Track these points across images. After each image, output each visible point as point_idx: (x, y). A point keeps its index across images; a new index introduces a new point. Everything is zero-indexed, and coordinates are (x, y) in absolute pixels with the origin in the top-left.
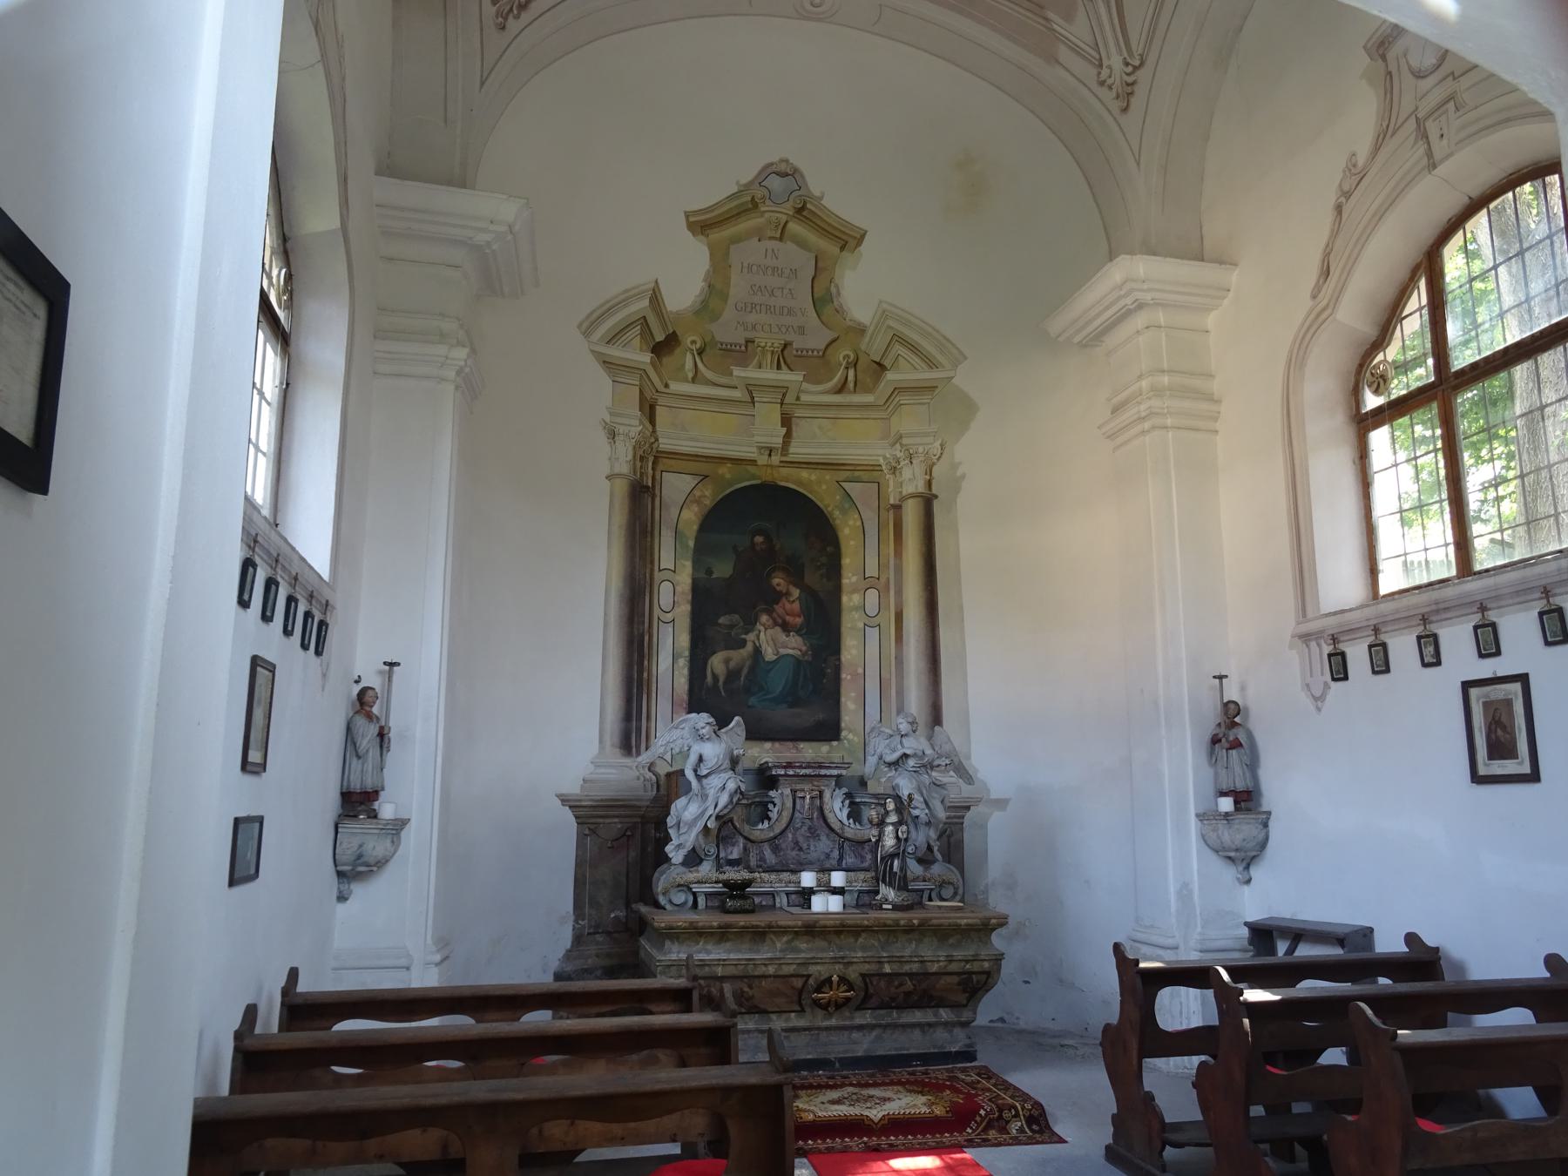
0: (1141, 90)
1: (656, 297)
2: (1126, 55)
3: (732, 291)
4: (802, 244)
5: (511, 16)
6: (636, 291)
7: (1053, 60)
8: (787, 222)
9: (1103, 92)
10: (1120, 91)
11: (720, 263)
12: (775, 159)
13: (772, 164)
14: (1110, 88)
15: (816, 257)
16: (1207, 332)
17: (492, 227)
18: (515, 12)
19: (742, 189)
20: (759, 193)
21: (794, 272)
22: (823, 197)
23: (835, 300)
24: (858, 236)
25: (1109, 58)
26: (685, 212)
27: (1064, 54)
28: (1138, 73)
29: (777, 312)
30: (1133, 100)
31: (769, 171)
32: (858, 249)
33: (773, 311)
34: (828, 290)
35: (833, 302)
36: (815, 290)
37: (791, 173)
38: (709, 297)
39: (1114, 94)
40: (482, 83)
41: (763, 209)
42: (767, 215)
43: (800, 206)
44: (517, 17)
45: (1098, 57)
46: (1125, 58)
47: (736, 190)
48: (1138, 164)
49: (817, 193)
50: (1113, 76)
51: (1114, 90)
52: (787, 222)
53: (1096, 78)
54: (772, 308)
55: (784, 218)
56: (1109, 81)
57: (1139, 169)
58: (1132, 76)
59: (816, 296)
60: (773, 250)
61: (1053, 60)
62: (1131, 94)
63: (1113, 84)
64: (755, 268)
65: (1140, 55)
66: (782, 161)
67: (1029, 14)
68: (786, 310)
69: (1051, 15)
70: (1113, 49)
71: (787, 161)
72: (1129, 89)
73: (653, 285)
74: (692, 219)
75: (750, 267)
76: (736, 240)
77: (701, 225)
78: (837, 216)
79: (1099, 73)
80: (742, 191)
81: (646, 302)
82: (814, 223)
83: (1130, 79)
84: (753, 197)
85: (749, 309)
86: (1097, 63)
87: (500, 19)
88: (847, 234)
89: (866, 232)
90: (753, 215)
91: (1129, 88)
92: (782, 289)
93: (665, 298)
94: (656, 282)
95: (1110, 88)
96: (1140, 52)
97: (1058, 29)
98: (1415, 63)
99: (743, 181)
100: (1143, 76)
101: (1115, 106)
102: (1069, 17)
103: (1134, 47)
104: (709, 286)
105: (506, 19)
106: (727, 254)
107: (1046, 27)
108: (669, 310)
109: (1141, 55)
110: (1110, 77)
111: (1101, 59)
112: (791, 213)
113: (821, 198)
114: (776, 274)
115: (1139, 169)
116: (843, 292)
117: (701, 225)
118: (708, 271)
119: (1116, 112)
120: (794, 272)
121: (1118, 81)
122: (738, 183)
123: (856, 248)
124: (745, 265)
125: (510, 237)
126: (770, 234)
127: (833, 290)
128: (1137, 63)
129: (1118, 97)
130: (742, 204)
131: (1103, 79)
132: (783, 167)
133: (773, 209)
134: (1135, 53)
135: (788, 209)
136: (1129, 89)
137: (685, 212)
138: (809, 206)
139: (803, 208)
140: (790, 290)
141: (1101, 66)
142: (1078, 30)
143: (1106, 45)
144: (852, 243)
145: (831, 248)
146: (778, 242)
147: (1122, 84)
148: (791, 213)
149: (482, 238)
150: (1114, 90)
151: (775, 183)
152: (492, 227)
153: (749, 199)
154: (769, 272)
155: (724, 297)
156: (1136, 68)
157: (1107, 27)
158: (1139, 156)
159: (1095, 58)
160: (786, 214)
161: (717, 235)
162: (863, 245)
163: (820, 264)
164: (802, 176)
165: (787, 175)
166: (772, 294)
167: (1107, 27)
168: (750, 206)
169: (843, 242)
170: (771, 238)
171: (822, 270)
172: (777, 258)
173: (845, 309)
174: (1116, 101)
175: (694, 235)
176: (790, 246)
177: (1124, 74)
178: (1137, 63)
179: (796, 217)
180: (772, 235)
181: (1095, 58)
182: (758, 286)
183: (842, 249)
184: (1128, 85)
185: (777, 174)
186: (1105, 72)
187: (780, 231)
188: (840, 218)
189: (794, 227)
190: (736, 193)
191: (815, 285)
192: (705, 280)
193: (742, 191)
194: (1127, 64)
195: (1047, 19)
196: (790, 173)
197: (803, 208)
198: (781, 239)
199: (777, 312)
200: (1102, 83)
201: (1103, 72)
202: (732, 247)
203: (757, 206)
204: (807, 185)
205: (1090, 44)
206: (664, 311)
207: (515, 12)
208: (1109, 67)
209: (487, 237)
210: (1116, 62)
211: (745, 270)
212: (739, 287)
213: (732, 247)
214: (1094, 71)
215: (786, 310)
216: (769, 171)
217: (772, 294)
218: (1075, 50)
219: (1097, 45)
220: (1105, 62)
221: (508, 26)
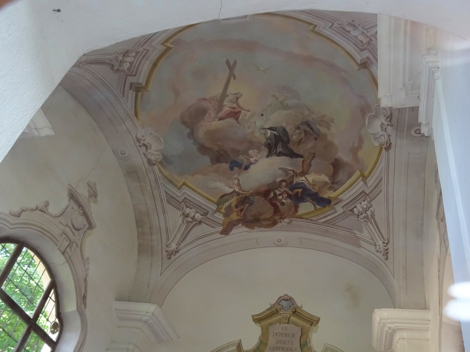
0: (390, 251)
1: (240, 346)
2: (383, 240)
3: (269, 342)
4: (296, 324)
5: (172, 255)
6: (232, 343)
7: (359, 246)
8: (290, 317)
9: (379, 254)
10: (384, 252)
11: (265, 333)
12: (283, 295)
13: (281, 297)
14: (380, 252)
15: (302, 329)
16: (428, 340)
17: (147, 314)
18: (174, 254)
19: (272, 306)
20: (278, 307)
21: (293, 335)
22: (302, 307)
23: (308, 344)
24: (317, 320)
25: (378, 242)
26: (252, 316)
27: (363, 243)
28: (388, 245)
29: (286, 350)
30: (388, 255)
31: (281, 299)
32: (317, 325)
33: (284, 350)
34: (306, 340)
35: (307, 345)
36: (301, 341)
37: (289, 299)
38: (260, 345)
39: (382, 254)
40: (161, 274)
41: (280, 313)
42: (282, 315)
43: (294, 310)
44: (175, 255)
45: (374, 242)
46: (383, 241)
47: (270, 307)
48: (394, 277)
49: (300, 305)
50: (380, 248)
51: (382, 253)
52: (290, 317)
53: (375, 250)
54: (284, 348)
55: (289, 315)
56: (380, 250)
57: (395, 279)
58: (386, 247)
59: (301, 343)
60: (285, 327)
61: (359, 246)
62: (387, 253)
63: (381, 251)
64: (278, 334)
65: (387, 239)
66: (285, 295)
67: (347, 233)
68: (289, 349)
69: (355, 232)
70: (378, 238)
71: (287, 295)
72: (386, 251)
73: (239, 341)
74: (254, 318)
75: (276, 334)
76: (271, 324)
77: (258, 319)
78: (308, 313)
79: (376, 248)
80: (272, 307)
81: (235, 347)
82: (300, 316)
83: (386, 248)
84: (276, 309)
85: (275, 349)
86: (374, 245)
87: (169, 256)
88: (312, 319)
89: (320, 318)
90: (277, 315)
91: (387, 251)
92: (289, 341)
93: (243, 346)
94: (240, 340)
95: (380, 252)
96: (387, 238)
97: (359, 236)
98: (236, 194)
99: (272, 303)
100: (390, 246)
101: (383, 258)
102: (361, 231)
103: (384, 236)
104: (260, 341)
105: (171, 256)
106: (268, 329)
107: (354, 236)
108: (244, 350)
109: (388, 239)
110: (380, 248)
111: (375, 243)
112: (291, 313)
113: (302, 307)
114: (286, 336)
115: (395, 279)
116: (312, 341)
117: (258, 319)
118: (261, 336)
119: (384, 260)
120: (293, 335)
121: (382, 250)
122: (270, 304)
123: (316, 324)
124: (275, 333)
125: (154, 318)
126: (284, 322)
127: (308, 341)
128: (387, 242)
129: (383, 255)
130: (272, 312)
131: (377, 250)
132: (286, 297)
133: (285, 312)
134: (385, 238)
135: (290, 312)
136: (386, 251)
137: (252, 316)
138: (297, 310)
139: (295, 311)
140: (292, 341)
141: (376, 245)
142: (365, 235)
143: (376, 238)
144: (315, 323)
145: (307, 325)
146: (287, 324)
147: (384, 250)
148: (291, 313)
149: (145, 318)
150: (382, 253)
151: (284, 303)
152: (147, 314)
153: (275, 309)
154: (284, 335)
155: (266, 345)
156: (387, 244)
157: (375, 232)
158: (394, 274)
159: (373, 243)
160: (290, 314)
161: (263, 323)
162: (319, 324)
163: (303, 331)
164: (294, 300)
165: (288, 300)
166: (284, 343)
167: (375, 232)
168: (276, 312)
169: (311, 323)
170: (284, 323)
171: (304, 334)
172: (287, 330)
173: (312, 348)
174: (383, 256)
175: (255, 323)
176: (291, 325)
177: (384, 247)
178: (387, 242)
179: (292, 315)
180: (284, 322)
181: (373, 243)
182: (279, 340)
183: (311, 325)
184: (386, 250)
185: (284, 300)
186: (378, 247)
187: (287, 320)
188: (310, 314)
189: (293, 319)
190: (270, 308)
191: (301, 339)
192: (259, 339)
193: (272, 307)
194: (384, 243)
195: (354, 233)
196: (289, 299)
197: (295, 311)
198: (288, 323)
199: (286, 350)
200: (378, 251)
201: (377, 247)
202: (270, 327)
203: (278, 312)
204: (295, 303)
205: (371, 239)
206: (242, 350)
207: (174, 254)
208: (379, 245)
209: (147, 318)
210: (380, 243)
211: (275, 335)
212: (272, 341)
213: (270, 327)
214: (374, 247)
215: (289, 349)
216: (281, 299)
217: (284, 343)
218: (366, 241)
219: (373, 239)
220: (377, 244)
221: (171, 257)
